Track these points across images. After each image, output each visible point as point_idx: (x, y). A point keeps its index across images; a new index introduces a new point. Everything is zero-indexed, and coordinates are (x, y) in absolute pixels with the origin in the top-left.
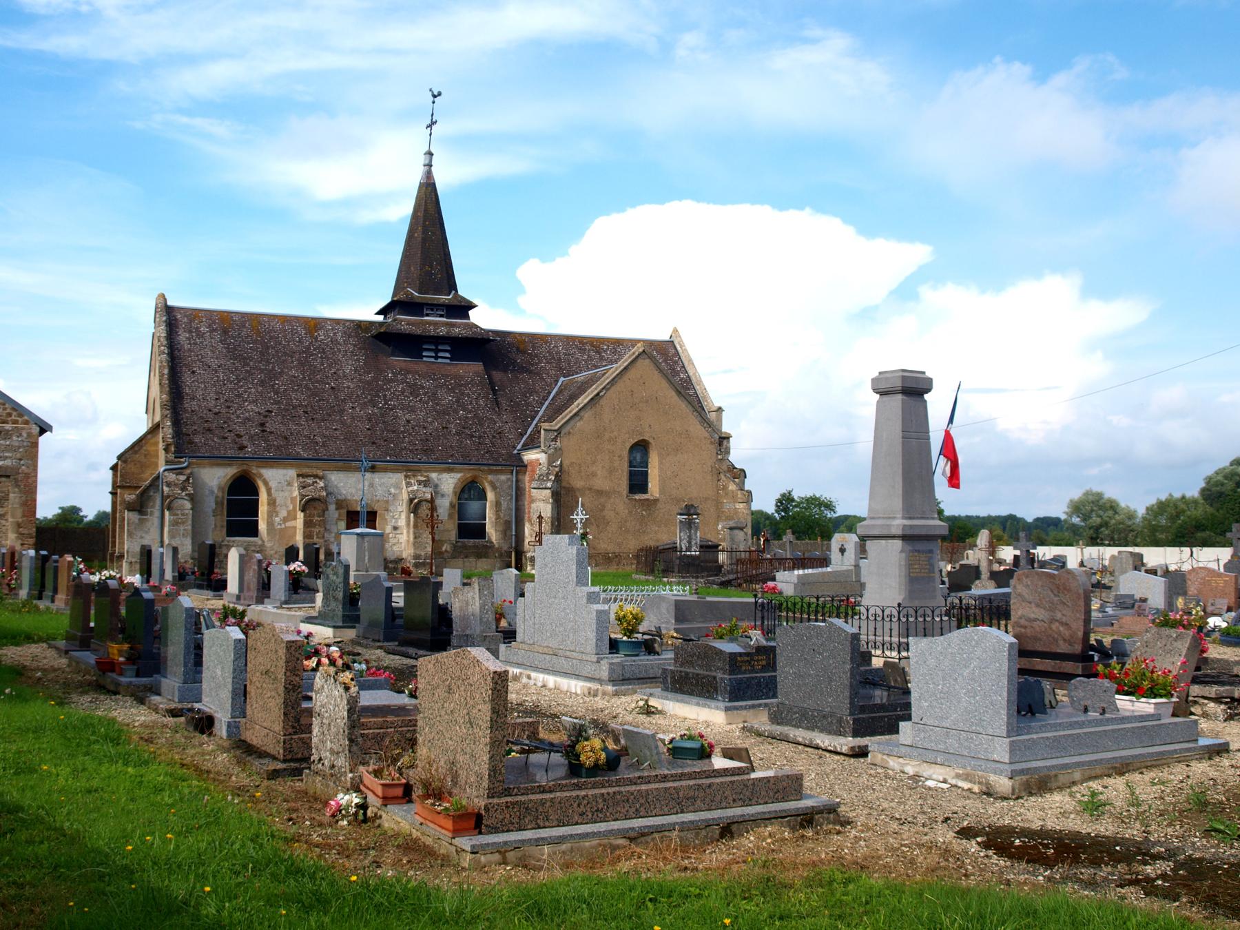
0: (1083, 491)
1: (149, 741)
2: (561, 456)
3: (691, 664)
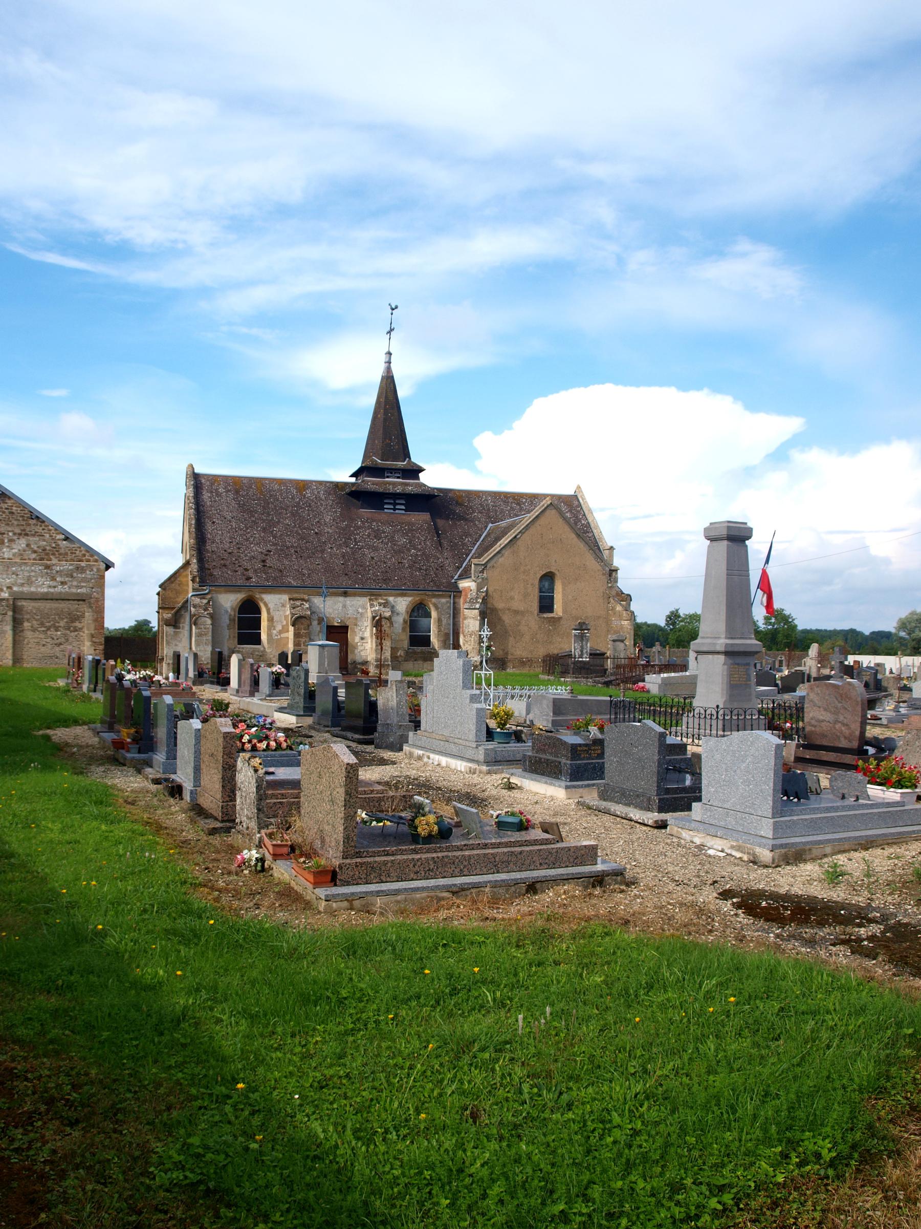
0: (909, 611)
1: (133, 803)
2: (487, 584)
3: (544, 751)
